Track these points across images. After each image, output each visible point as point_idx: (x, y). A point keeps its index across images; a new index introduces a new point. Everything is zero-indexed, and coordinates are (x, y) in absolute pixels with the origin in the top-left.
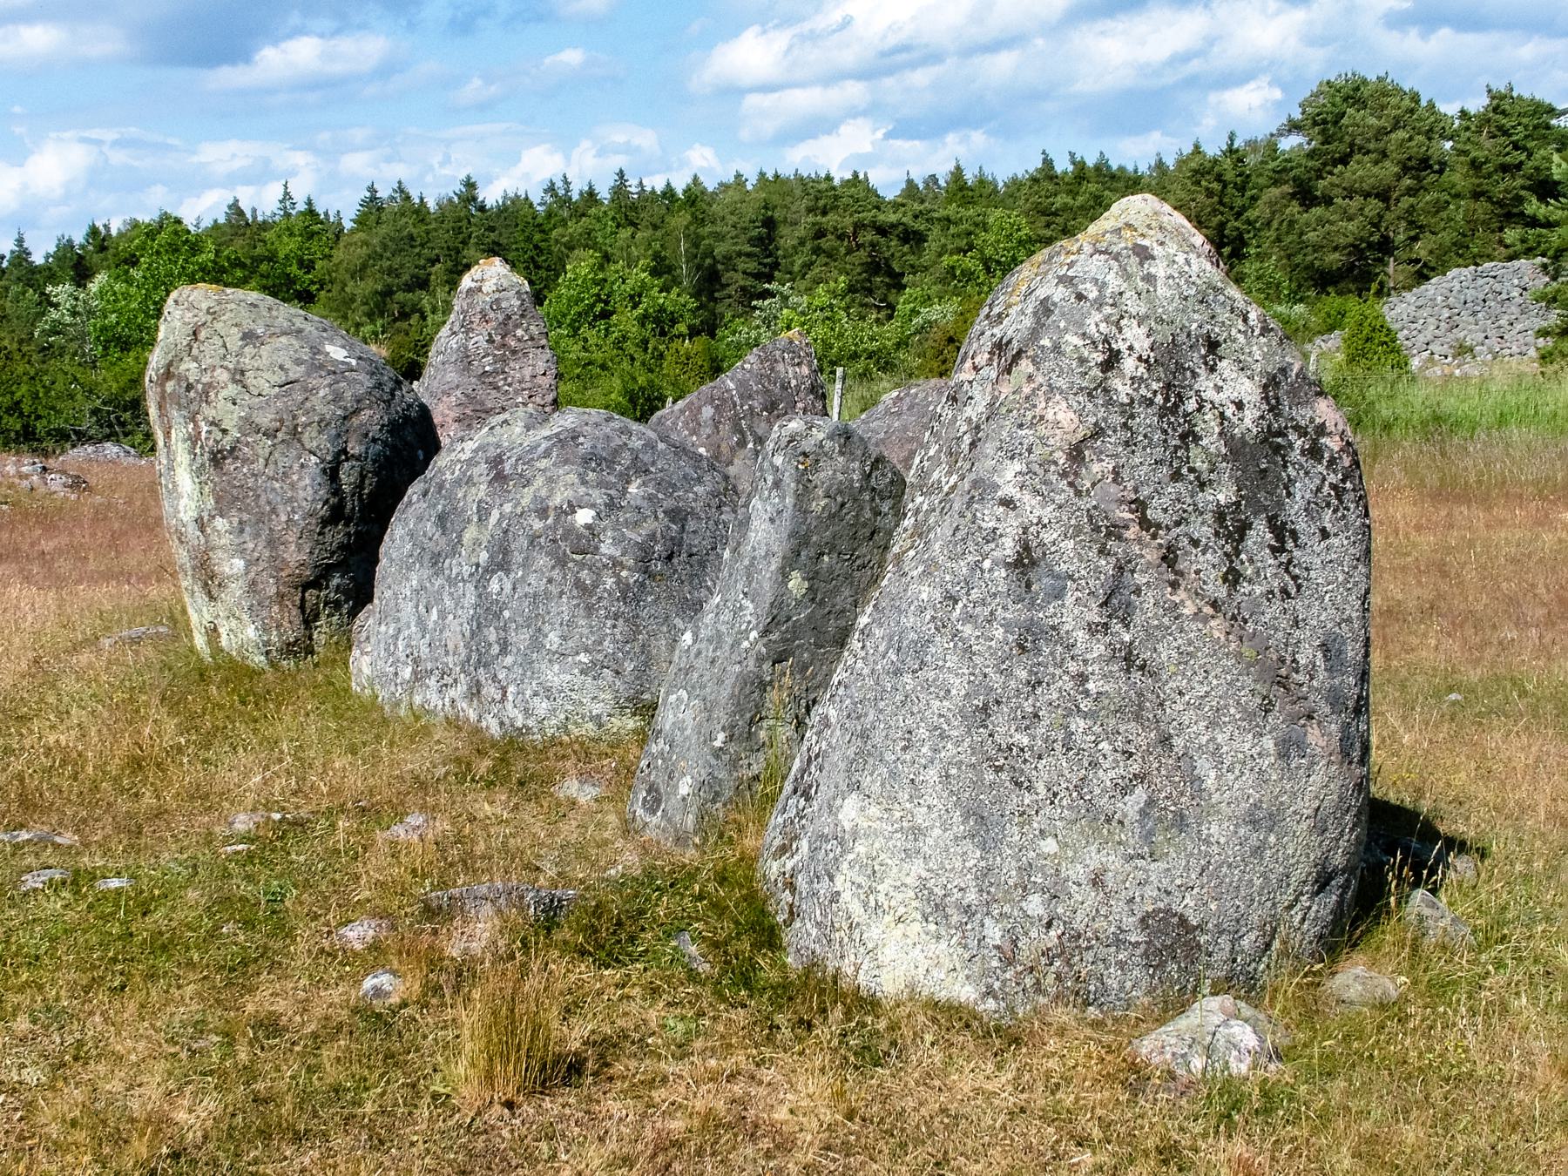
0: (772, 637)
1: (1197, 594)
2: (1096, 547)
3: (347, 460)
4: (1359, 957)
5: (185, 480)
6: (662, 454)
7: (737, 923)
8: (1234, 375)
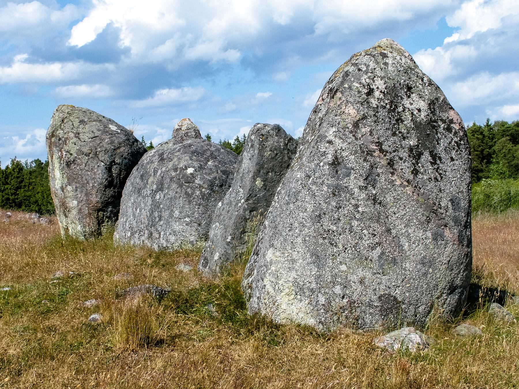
0: (250, 202)
1: (401, 177)
2: (362, 159)
3: (115, 165)
4: (469, 321)
5: (58, 174)
6: (223, 153)
7: (230, 300)
8: (417, 99)
